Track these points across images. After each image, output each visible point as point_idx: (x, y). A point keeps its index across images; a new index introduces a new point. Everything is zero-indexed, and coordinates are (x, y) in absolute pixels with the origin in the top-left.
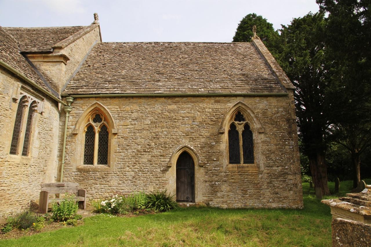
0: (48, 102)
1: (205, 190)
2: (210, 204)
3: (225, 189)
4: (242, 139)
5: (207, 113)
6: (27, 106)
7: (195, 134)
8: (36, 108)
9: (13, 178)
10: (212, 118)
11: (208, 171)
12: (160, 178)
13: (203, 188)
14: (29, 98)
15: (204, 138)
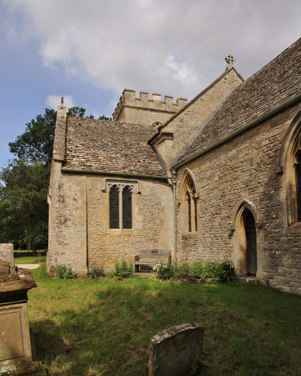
0: (147, 182)
1: (265, 262)
2: (270, 282)
3: (287, 263)
5: (263, 148)
6: (120, 191)
7: (253, 183)
8: (132, 191)
9: (117, 246)
10: (270, 154)
11: (268, 234)
12: (228, 244)
13: (263, 258)
14: (120, 185)
15: (263, 186)
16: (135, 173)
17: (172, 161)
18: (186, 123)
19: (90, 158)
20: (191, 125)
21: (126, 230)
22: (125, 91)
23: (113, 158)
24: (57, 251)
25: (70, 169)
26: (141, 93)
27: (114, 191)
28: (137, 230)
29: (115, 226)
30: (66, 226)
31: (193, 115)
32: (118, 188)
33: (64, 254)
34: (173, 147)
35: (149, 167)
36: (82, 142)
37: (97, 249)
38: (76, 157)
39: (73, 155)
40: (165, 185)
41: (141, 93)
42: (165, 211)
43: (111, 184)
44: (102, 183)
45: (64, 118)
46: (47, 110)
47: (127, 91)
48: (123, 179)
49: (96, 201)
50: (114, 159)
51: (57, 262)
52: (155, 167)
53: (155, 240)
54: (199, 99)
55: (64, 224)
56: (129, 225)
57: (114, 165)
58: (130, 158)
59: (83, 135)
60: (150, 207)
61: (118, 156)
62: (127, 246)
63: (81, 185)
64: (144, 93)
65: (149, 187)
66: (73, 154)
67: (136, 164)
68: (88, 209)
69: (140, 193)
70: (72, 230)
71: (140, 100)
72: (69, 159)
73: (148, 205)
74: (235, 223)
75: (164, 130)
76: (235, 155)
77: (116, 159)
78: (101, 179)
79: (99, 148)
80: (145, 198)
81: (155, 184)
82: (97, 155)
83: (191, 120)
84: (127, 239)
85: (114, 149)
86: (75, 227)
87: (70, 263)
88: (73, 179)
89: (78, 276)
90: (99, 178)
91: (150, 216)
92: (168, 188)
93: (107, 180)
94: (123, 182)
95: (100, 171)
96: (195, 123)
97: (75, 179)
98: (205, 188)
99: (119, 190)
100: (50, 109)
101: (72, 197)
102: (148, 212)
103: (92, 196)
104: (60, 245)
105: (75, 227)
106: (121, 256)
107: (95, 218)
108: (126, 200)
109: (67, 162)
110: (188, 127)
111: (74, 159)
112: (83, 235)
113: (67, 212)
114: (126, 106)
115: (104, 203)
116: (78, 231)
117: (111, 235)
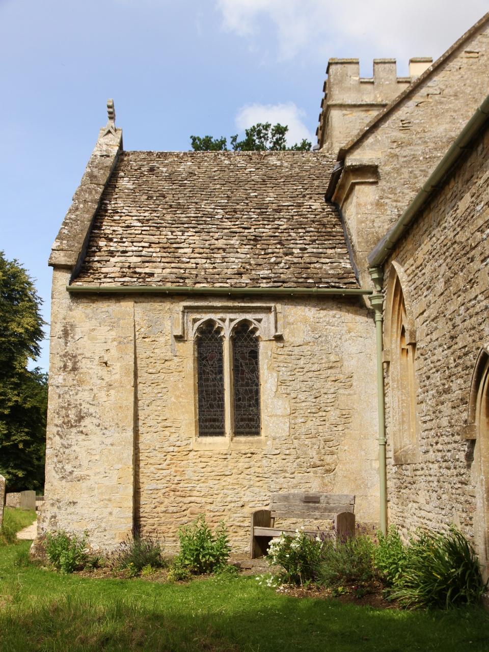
0: (299, 307)
4: (264, 305)
6: (224, 336)
8: (257, 334)
9: (216, 482)
14: (223, 320)
16: (264, 285)
17: (375, 244)
18: (419, 130)
19: (154, 255)
20: (434, 135)
21: (242, 439)
22: (330, 64)
23: (219, 249)
24: (56, 497)
25: (94, 285)
26: (375, 63)
27: (208, 335)
28: (274, 439)
29: (212, 430)
30: (82, 432)
31: (441, 103)
32: (220, 329)
33: (74, 503)
34: (379, 205)
35: (312, 266)
36: (146, 214)
37: (164, 491)
38: (119, 254)
39: (112, 249)
40: (356, 313)
41: (375, 63)
42: (354, 384)
43: (199, 320)
44: (171, 318)
45: (108, 156)
46: (194, 139)
47: (337, 63)
48: (230, 304)
49: (159, 366)
50: (221, 251)
51: (55, 524)
52: (330, 265)
53: (327, 467)
54: (463, 54)
55: (76, 426)
56: (218, 427)
57: (215, 268)
58: (265, 247)
59: (152, 197)
60: (310, 374)
61: (232, 242)
62: (246, 483)
63: (119, 326)
64: (385, 63)
65: (305, 320)
66: (113, 246)
67: (279, 260)
68: (140, 387)
69: (279, 338)
70: (96, 440)
71: (373, 83)
72: (99, 261)
73: (305, 370)
74: (474, 418)
75: (350, 161)
76: (468, 208)
77: (224, 250)
78: (172, 306)
79: (186, 225)
80: (296, 352)
81: (323, 313)
82: (175, 246)
83: (434, 120)
84: (246, 465)
85: (228, 224)
86: (104, 434)
87: (89, 528)
88: (99, 311)
89: (100, 562)
90: (167, 305)
91: (311, 399)
92: (365, 319)
93: (185, 308)
94: (232, 312)
95: (169, 285)
96: (447, 126)
97: (103, 310)
98: (425, 314)
99: (222, 334)
100: (202, 137)
101: (97, 358)
102: (304, 389)
103: (149, 353)
104: (64, 481)
105: (104, 434)
106: (229, 510)
107: (159, 408)
108: (244, 358)
109: (91, 268)
110: (426, 142)
111: (113, 260)
112: (125, 455)
113: (84, 396)
114: (335, 106)
115: (180, 369)
116: (112, 445)
117: (202, 453)
